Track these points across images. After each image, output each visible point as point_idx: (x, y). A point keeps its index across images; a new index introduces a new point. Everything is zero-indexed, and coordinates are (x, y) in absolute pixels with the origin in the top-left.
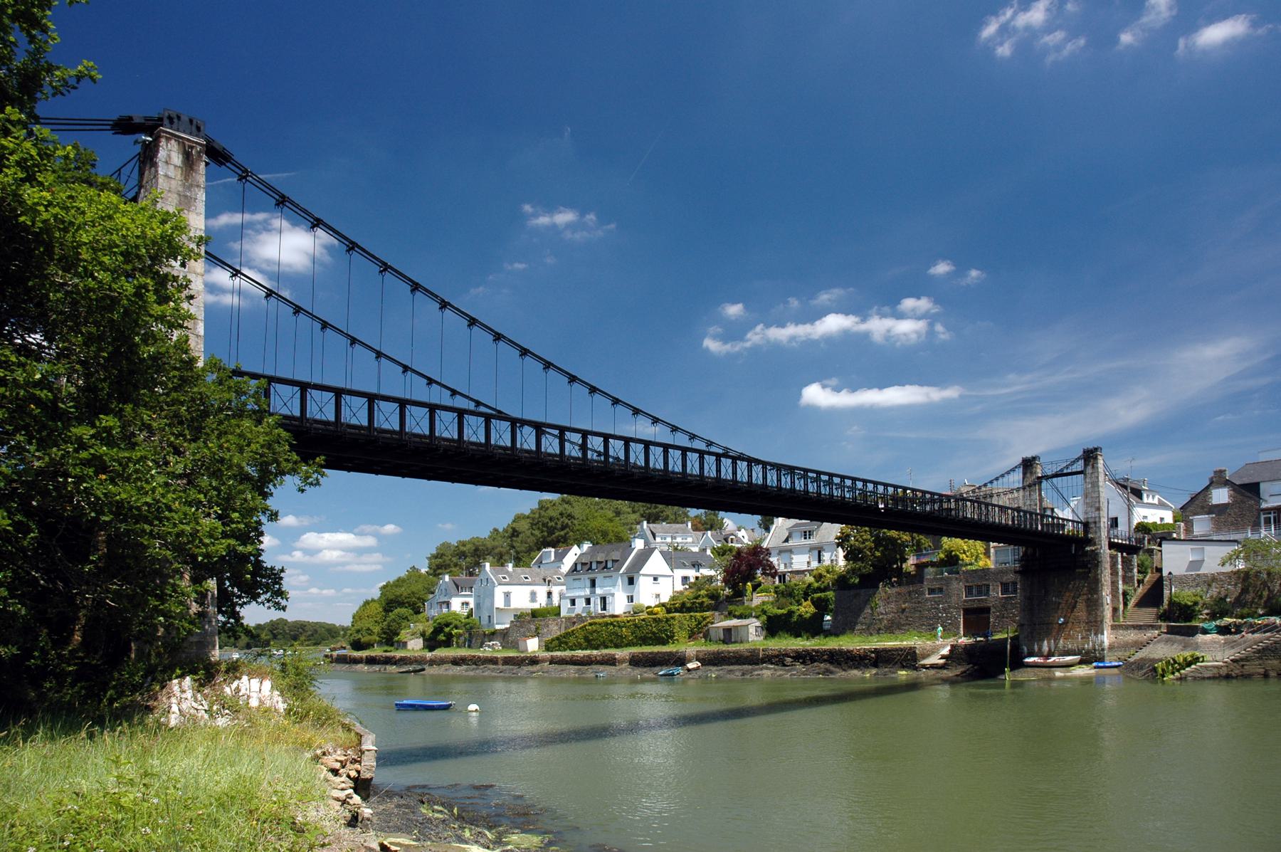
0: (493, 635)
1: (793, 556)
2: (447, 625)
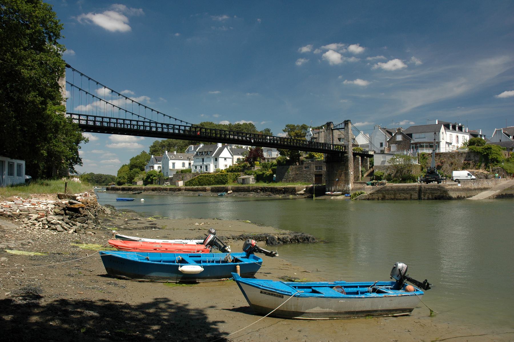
0: (167, 180)
1: (272, 152)
2: (151, 175)
